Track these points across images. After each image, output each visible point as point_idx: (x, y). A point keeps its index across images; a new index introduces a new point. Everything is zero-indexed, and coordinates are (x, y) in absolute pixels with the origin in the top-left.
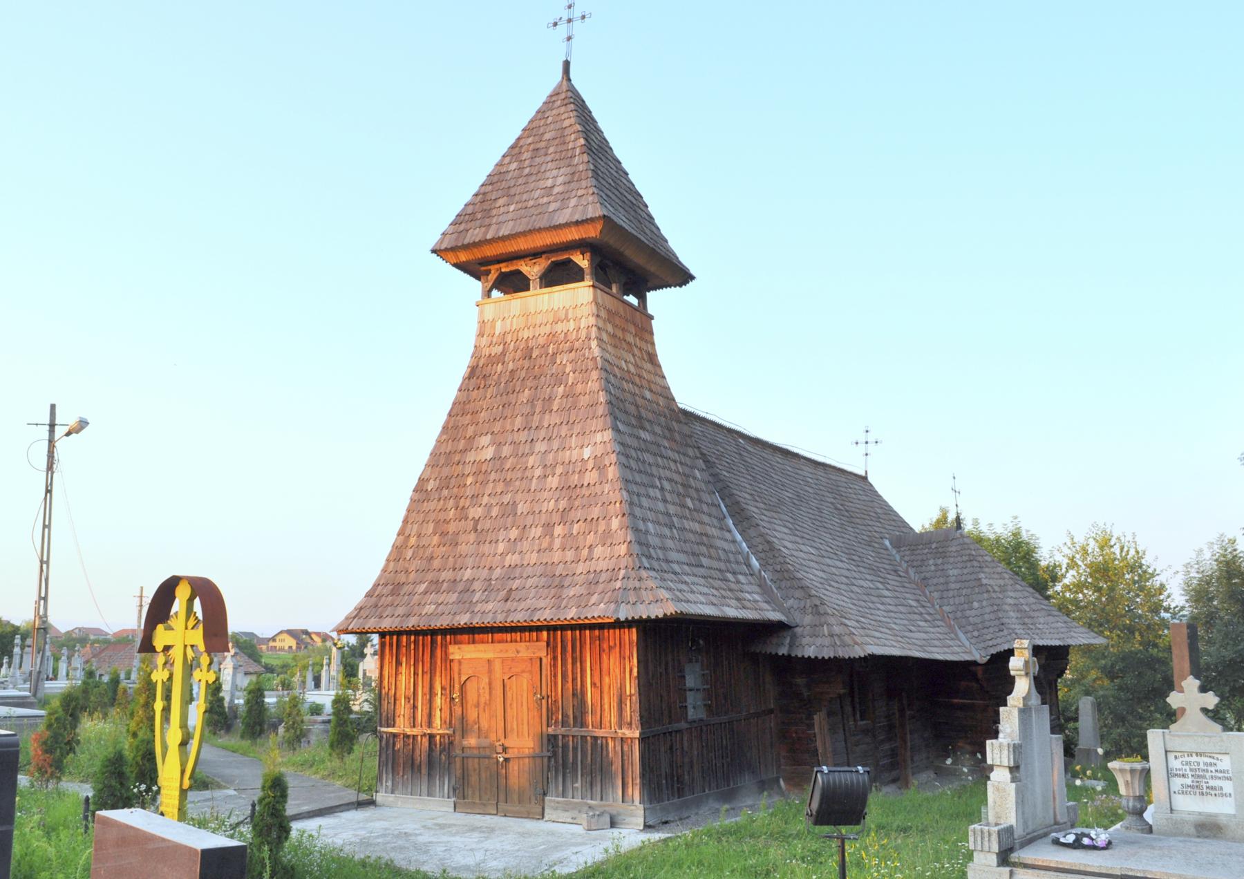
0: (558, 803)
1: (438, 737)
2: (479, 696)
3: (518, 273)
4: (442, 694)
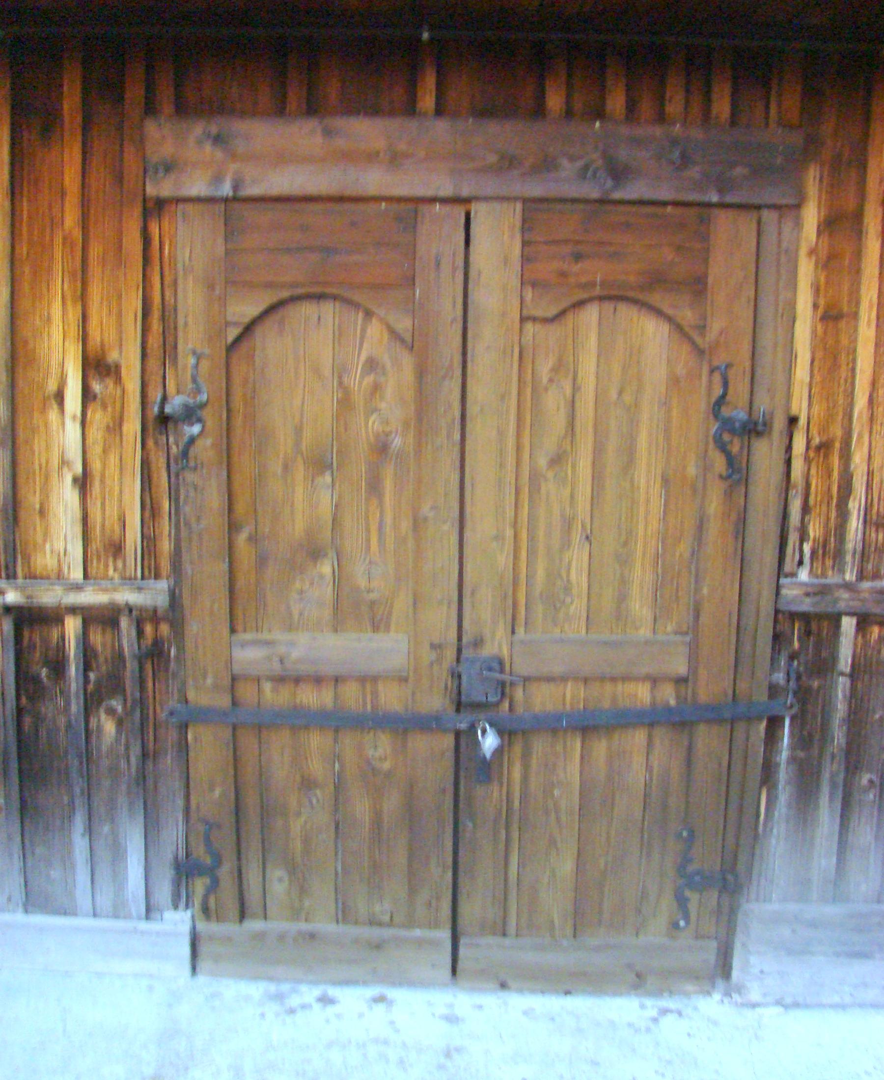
0: (813, 924)
1: (72, 626)
2: (345, 403)
3: (91, 694)
4: (87, 395)
